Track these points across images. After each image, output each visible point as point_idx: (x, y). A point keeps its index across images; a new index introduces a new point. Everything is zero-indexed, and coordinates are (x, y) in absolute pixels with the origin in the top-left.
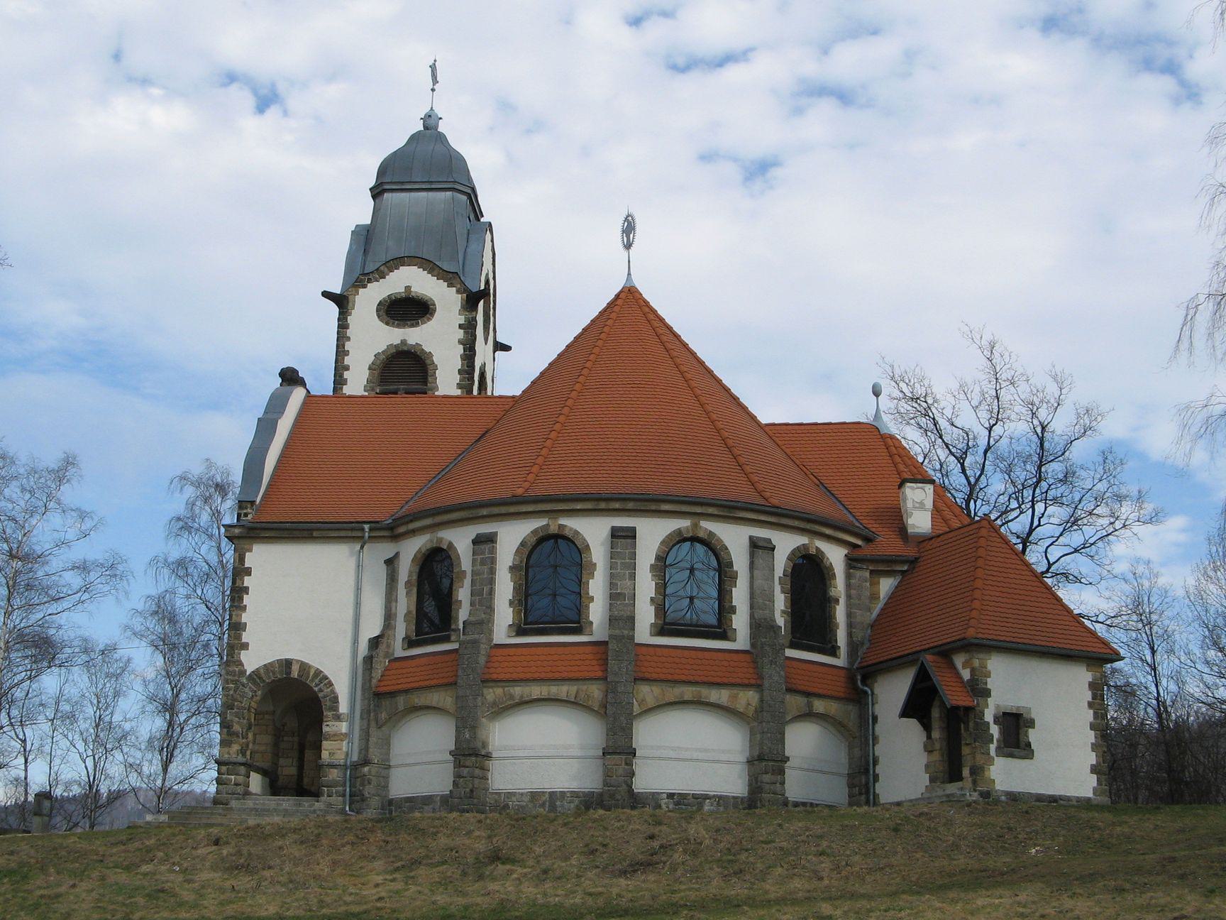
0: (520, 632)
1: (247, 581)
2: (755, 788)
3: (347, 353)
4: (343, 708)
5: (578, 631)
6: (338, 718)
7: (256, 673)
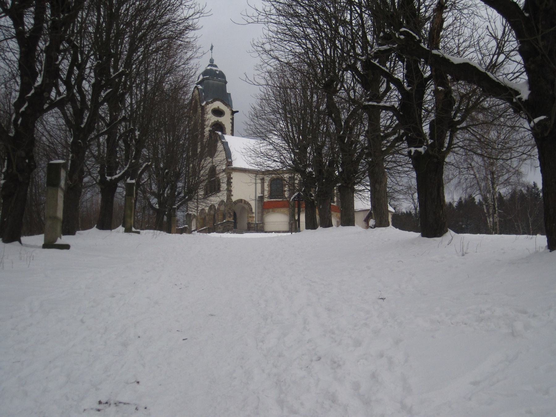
4: (254, 211)
6: (253, 213)
7: (235, 201)
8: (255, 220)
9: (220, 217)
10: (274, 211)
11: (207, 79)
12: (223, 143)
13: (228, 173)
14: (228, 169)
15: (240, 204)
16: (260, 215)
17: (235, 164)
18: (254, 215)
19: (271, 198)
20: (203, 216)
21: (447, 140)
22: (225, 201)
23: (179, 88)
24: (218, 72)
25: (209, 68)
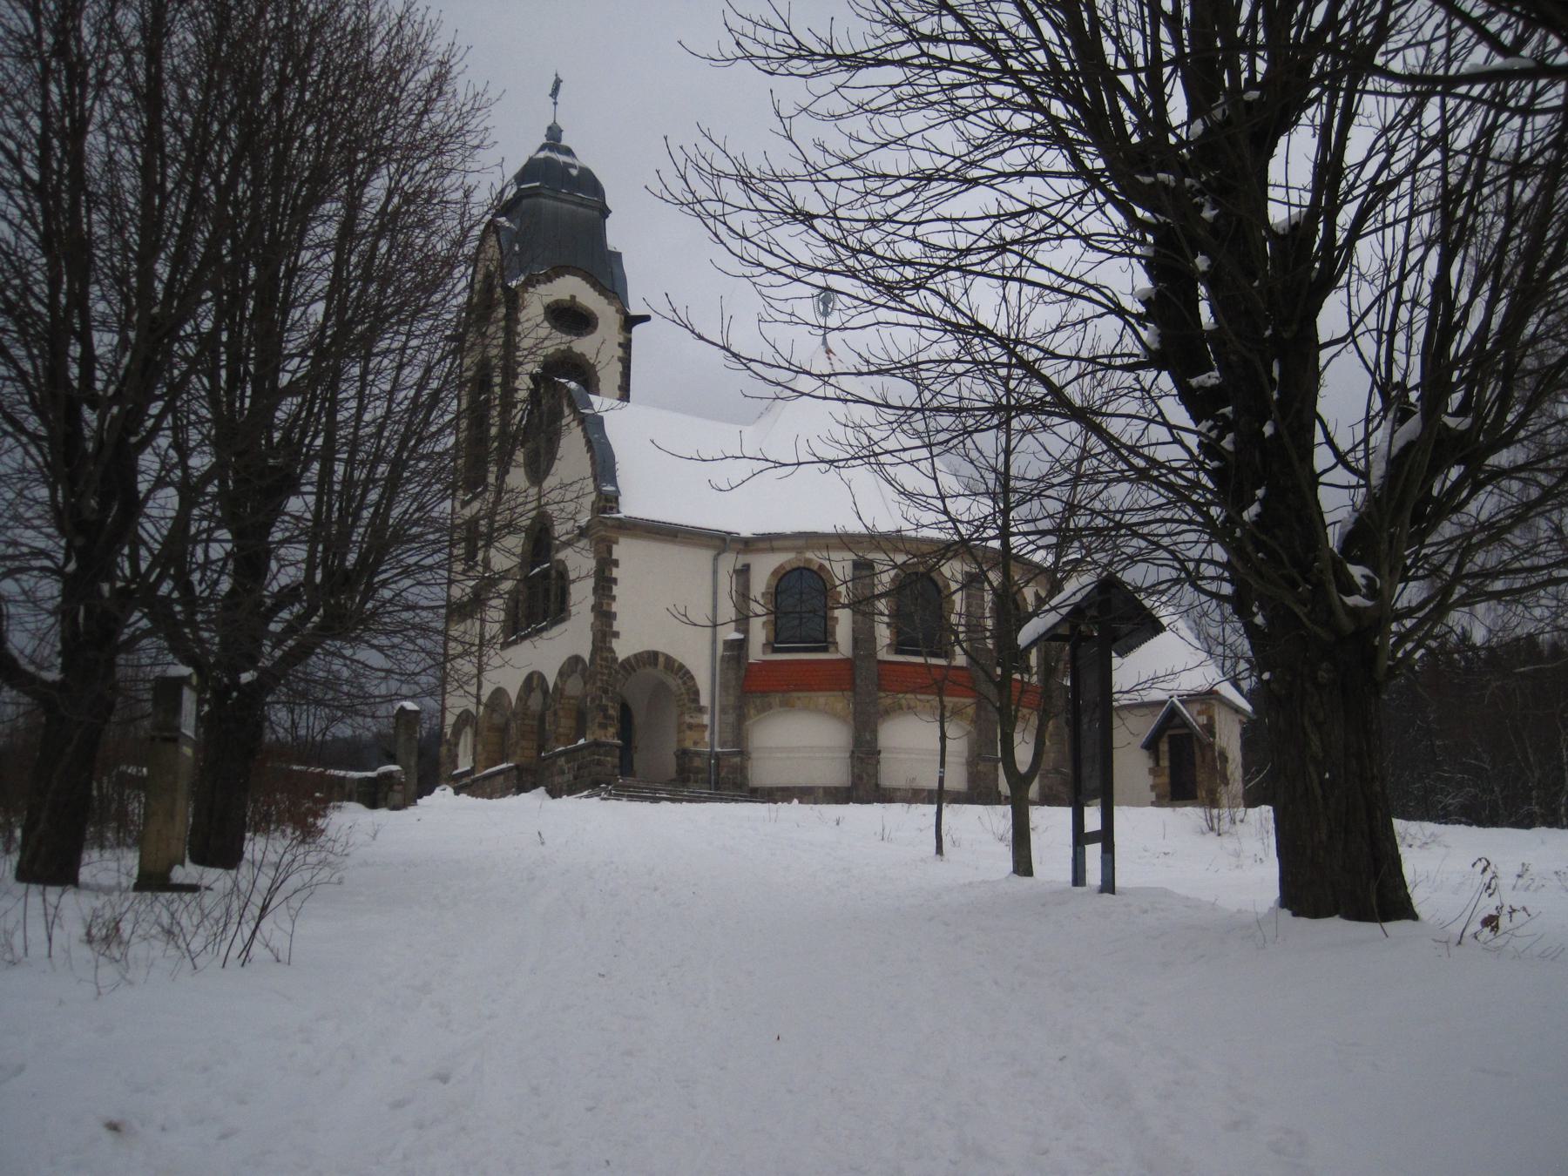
0: (899, 652)
1: (615, 573)
2: (857, 778)
3: (620, 359)
4: (705, 700)
5: (825, 650)
6: (701, 710)
7: (628, 660)
8: (709, 739)
9: (566, 724)
10: (788, 705)
11: (534, 193)
12: (583, 420)
13: (603, 539)
14: (602, 523)
15: (649, 670)
16: (731, 718)
17: (632, 506)
18: (706, 719)
19: (776, 651)
20: (497, 719)
21: (1464, 494)
22: (587, 657)
23: (360, 35)
24: (574, 172)
25: (542, 155)
